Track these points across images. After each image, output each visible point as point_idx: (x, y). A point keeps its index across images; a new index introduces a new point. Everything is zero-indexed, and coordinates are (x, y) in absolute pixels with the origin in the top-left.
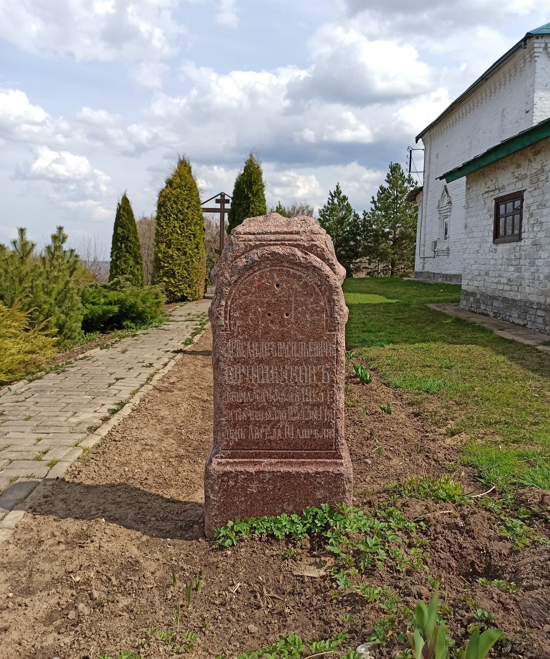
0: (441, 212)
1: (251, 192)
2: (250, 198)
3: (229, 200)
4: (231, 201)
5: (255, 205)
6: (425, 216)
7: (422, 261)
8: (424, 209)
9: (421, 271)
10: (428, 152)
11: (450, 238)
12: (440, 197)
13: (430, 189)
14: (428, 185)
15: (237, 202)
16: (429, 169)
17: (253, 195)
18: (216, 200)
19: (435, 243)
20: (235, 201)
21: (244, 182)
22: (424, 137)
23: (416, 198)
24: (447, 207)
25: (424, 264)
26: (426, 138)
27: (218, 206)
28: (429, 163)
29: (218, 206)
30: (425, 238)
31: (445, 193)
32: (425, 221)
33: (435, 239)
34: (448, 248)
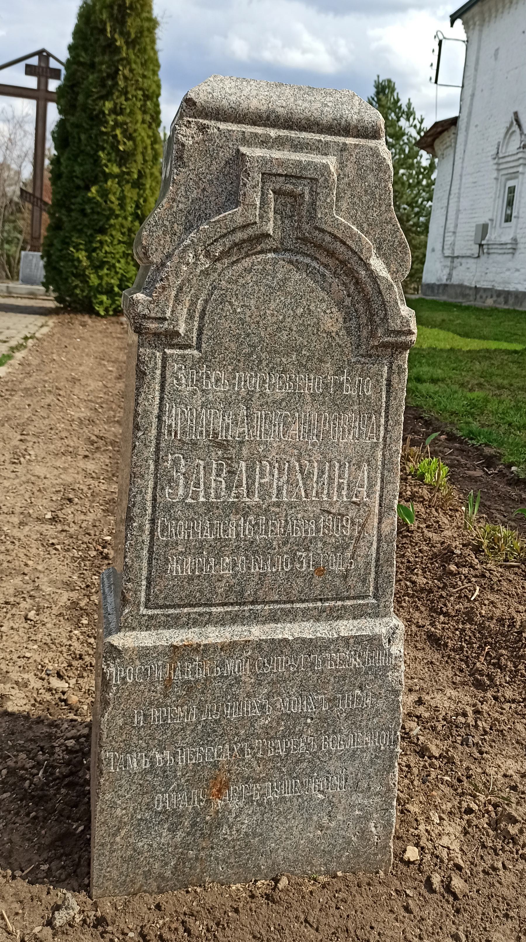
0: (502, 167)
1: (122, 34)
2: (118, 50)
3: (59, 71)
4: (63, 72)
5: (131, 70)
6: (461, 176)
7: (449, 264)
8: (458, 162)
9: (444, 281)
10: (474, 47)
11: (521, 220)
12: (502, 136)
13: (474, 121)
14: (470, 114)
15: (84, 58)
16: (475, 81)
17: (127, 43)
18: (27, 66)
19: (484, 229)
20: (78, 55)
21: (104, 7)
22: (468, 15)
23: (437, 142)
24: (520, 155)
25: (452, 268)
26: (473, 17)
27: (32, 82)
28: (476, 70)
29: (32, 82)
30: (457, 218)
31: (515, 127)
32: (460, 184)
33: (484, 219)
34: (515, 241)
